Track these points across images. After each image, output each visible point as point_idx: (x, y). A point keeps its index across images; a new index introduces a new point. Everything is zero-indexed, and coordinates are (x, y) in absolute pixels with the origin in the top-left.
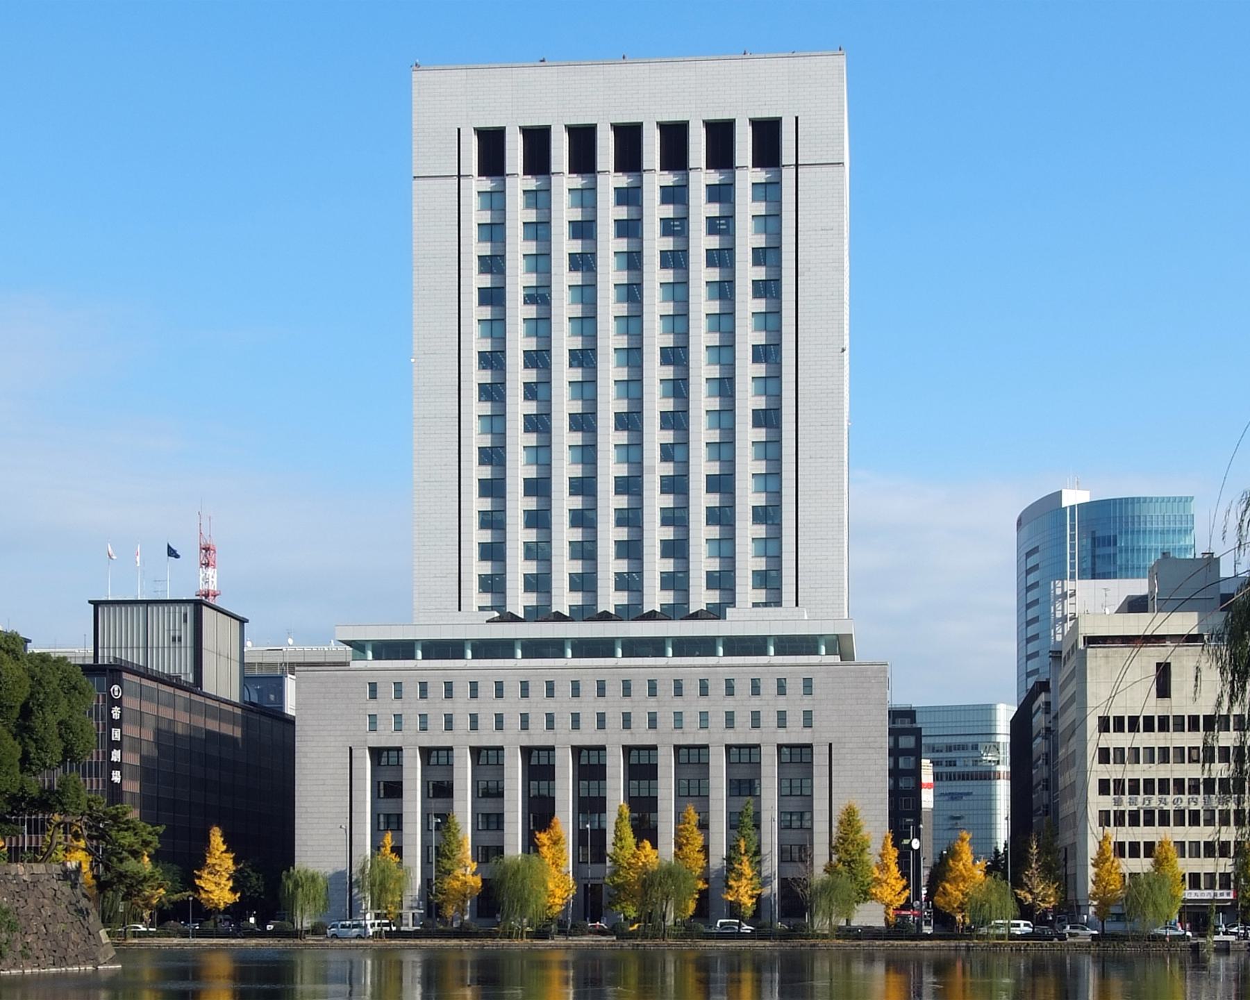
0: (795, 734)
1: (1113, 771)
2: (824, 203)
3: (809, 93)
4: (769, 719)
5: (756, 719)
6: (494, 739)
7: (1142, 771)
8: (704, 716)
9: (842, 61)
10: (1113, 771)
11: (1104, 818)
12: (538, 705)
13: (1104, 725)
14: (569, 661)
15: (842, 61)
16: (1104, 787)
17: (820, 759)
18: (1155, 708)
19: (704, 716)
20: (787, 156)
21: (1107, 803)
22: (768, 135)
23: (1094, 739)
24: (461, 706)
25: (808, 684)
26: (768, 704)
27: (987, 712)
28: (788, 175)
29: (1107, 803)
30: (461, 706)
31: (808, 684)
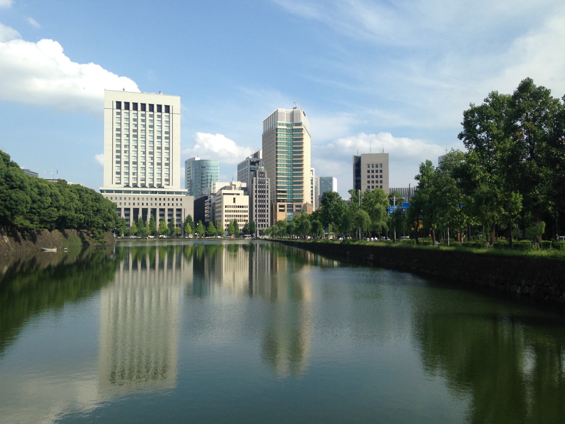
0: (179, 207)
1: (227, 214)
2: (177, 120)
3: (174, 102)
4: (175, 204)
5: (138, 204)
6: (163, 207)
7: (231, 214)
8: (156, 204)
9: (179, 97)
10: (227, 214)
11: (226, 211)
12: (171, 202)
13: (226, 207)
14: (141, 194)
15: (179, 97)
16: (226, 211)
17: (183, 211)
18: (234, 204)
19: (156, 204)
20: (171, 111)
21: (226, 218)
22: (167, 107)
23: (225, 209)
24: (123, 201)
25: (181, 199)
26: (149, 202)
27: (103, 186)
28: (171, 115)
29: (226, 218)
30: (123, 201)
31: (181, 199)
